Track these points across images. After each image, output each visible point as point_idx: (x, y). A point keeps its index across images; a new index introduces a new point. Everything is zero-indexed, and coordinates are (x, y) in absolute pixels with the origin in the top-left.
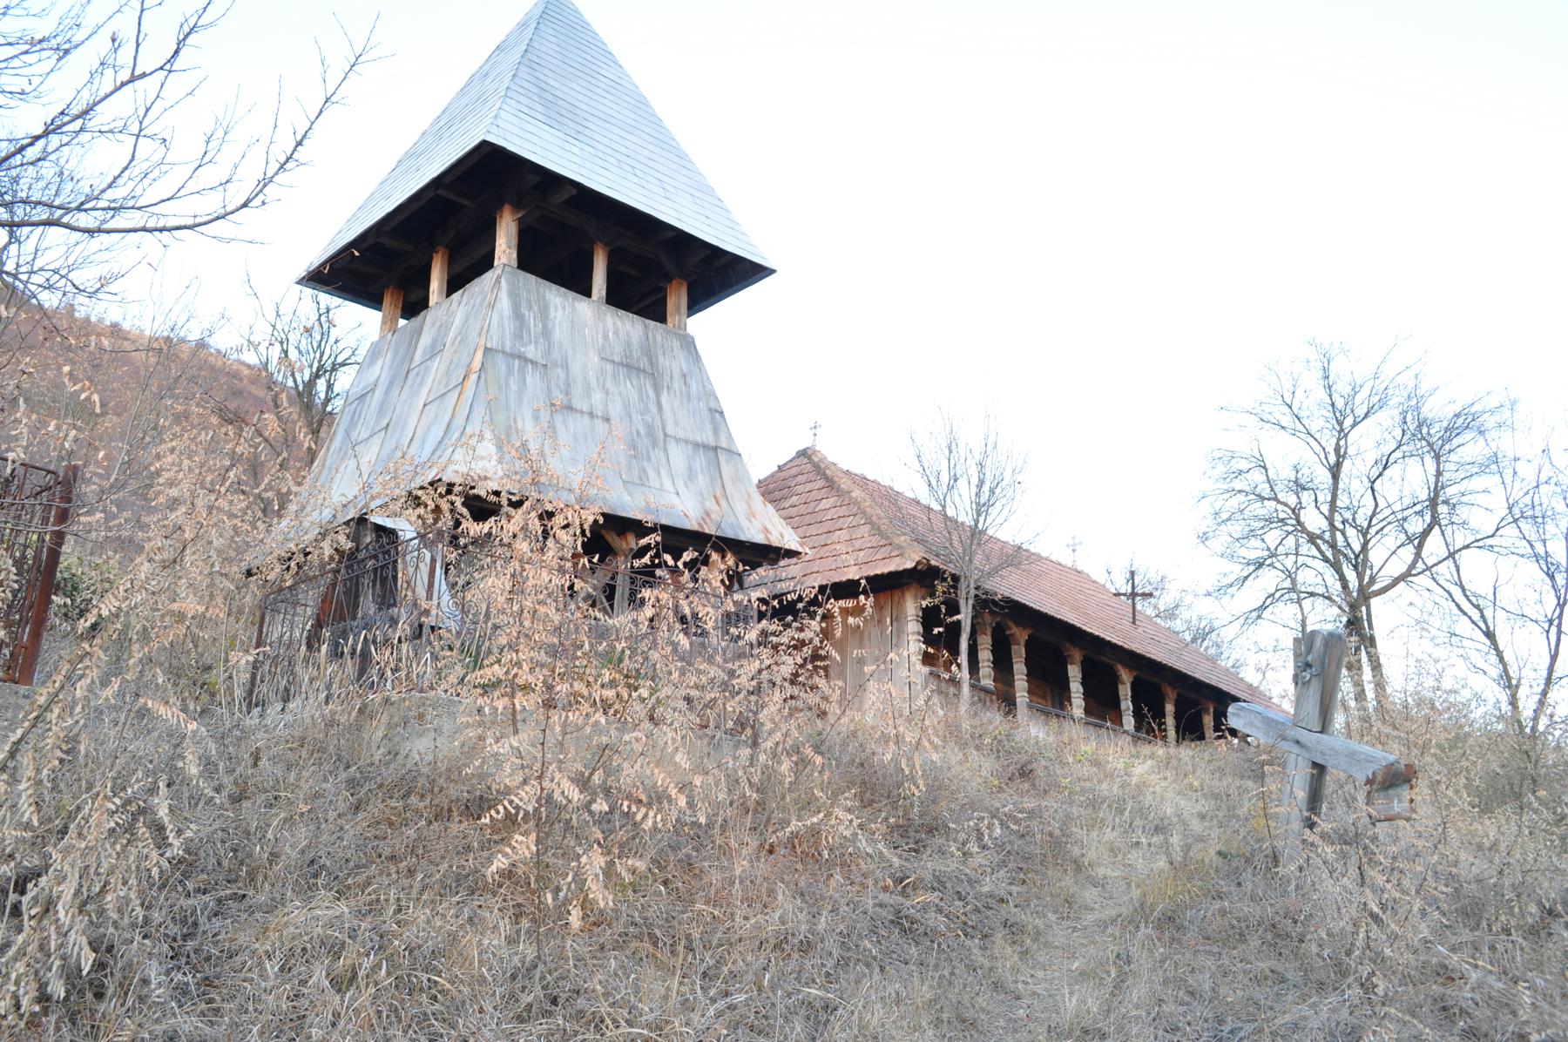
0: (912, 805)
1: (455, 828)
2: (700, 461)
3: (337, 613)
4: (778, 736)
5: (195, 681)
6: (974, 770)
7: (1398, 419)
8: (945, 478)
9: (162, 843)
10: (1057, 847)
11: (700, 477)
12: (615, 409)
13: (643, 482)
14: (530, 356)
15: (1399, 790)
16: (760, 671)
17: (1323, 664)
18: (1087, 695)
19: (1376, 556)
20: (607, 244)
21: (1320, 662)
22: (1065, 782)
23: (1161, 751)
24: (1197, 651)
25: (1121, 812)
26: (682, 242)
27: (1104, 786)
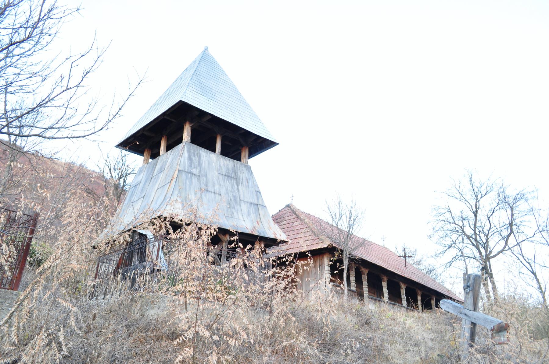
0: (327, 335)
1: (164, 343)
2: (252, 209)
3: (124, 263)
4: (279, 310)
5: (73, 287)
6: (349, 322)
7: (497, 196)
8: (338, 215)
9: (60, 350)
10: (379, 351)
11: (252, 214)
12: (223, 191)
13: (232, 216)
14: (194, 173)
15: (503, 333)
16: (273, 287)
17: (473, 286)
18: (389, 293)
19: (491, 244)
20: (221, 135)
21: (472, 285)
22: (382, 326)
23: (416, 314)
24: (429, 277)
25: (402, 338)
26: (247, 134)
27: (396, 328)
